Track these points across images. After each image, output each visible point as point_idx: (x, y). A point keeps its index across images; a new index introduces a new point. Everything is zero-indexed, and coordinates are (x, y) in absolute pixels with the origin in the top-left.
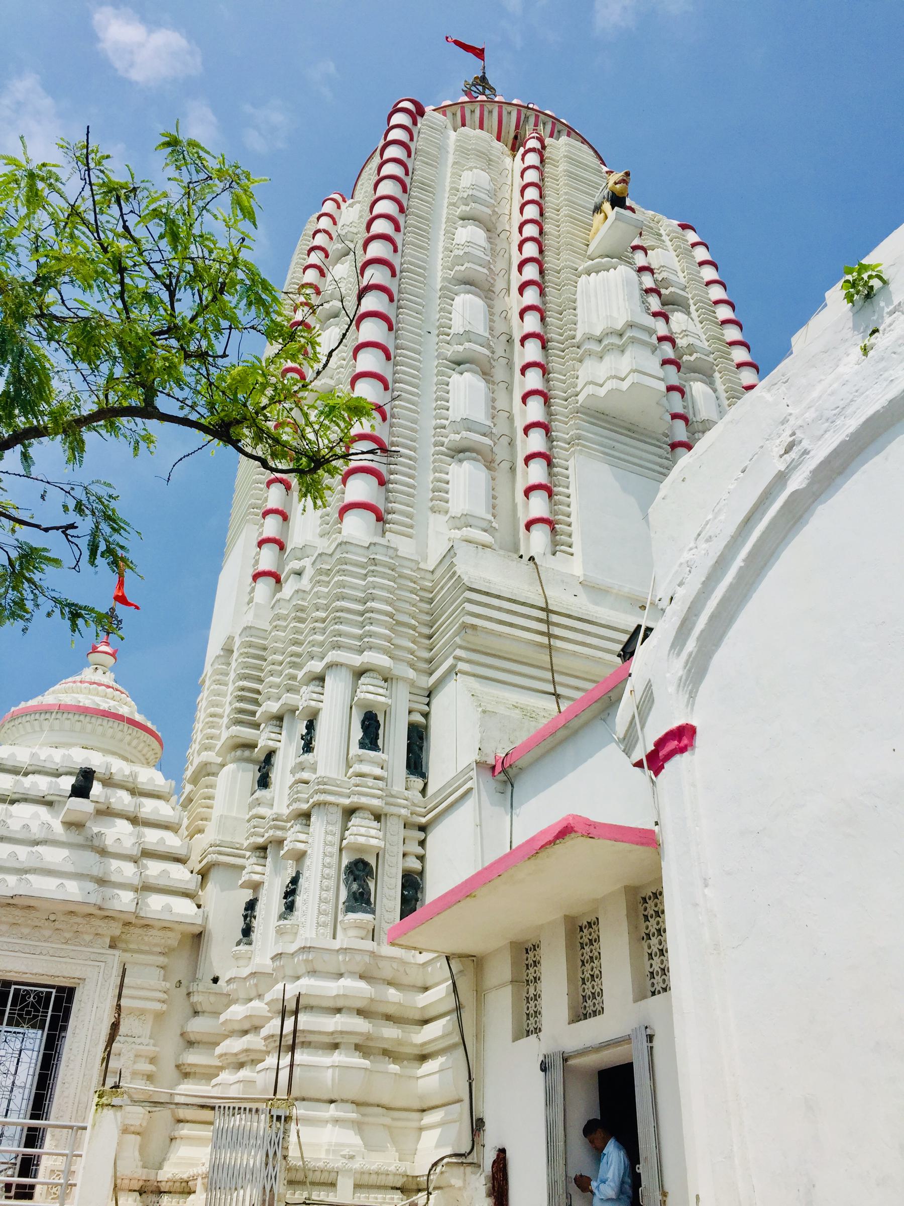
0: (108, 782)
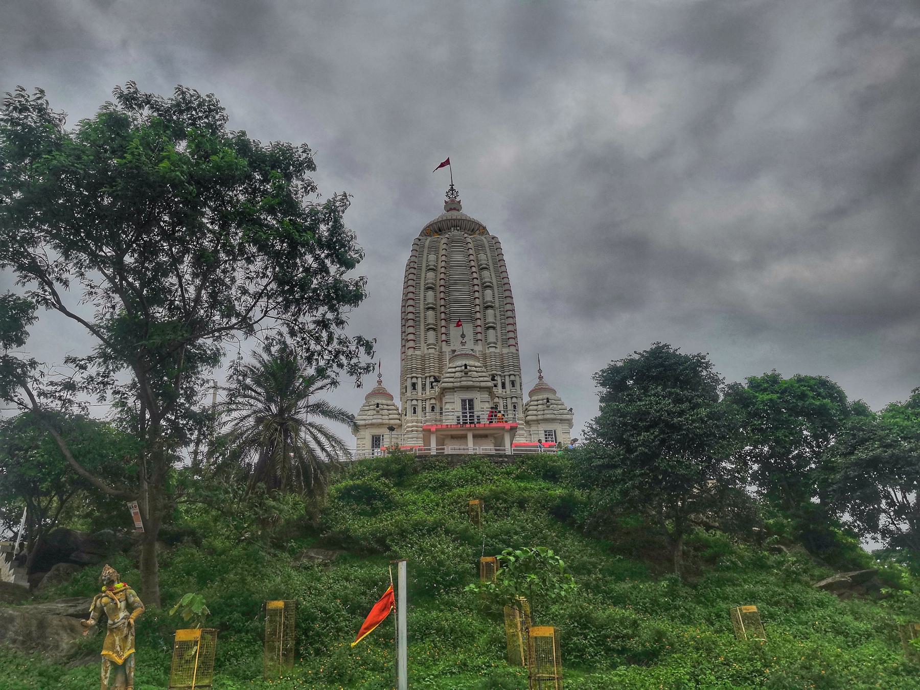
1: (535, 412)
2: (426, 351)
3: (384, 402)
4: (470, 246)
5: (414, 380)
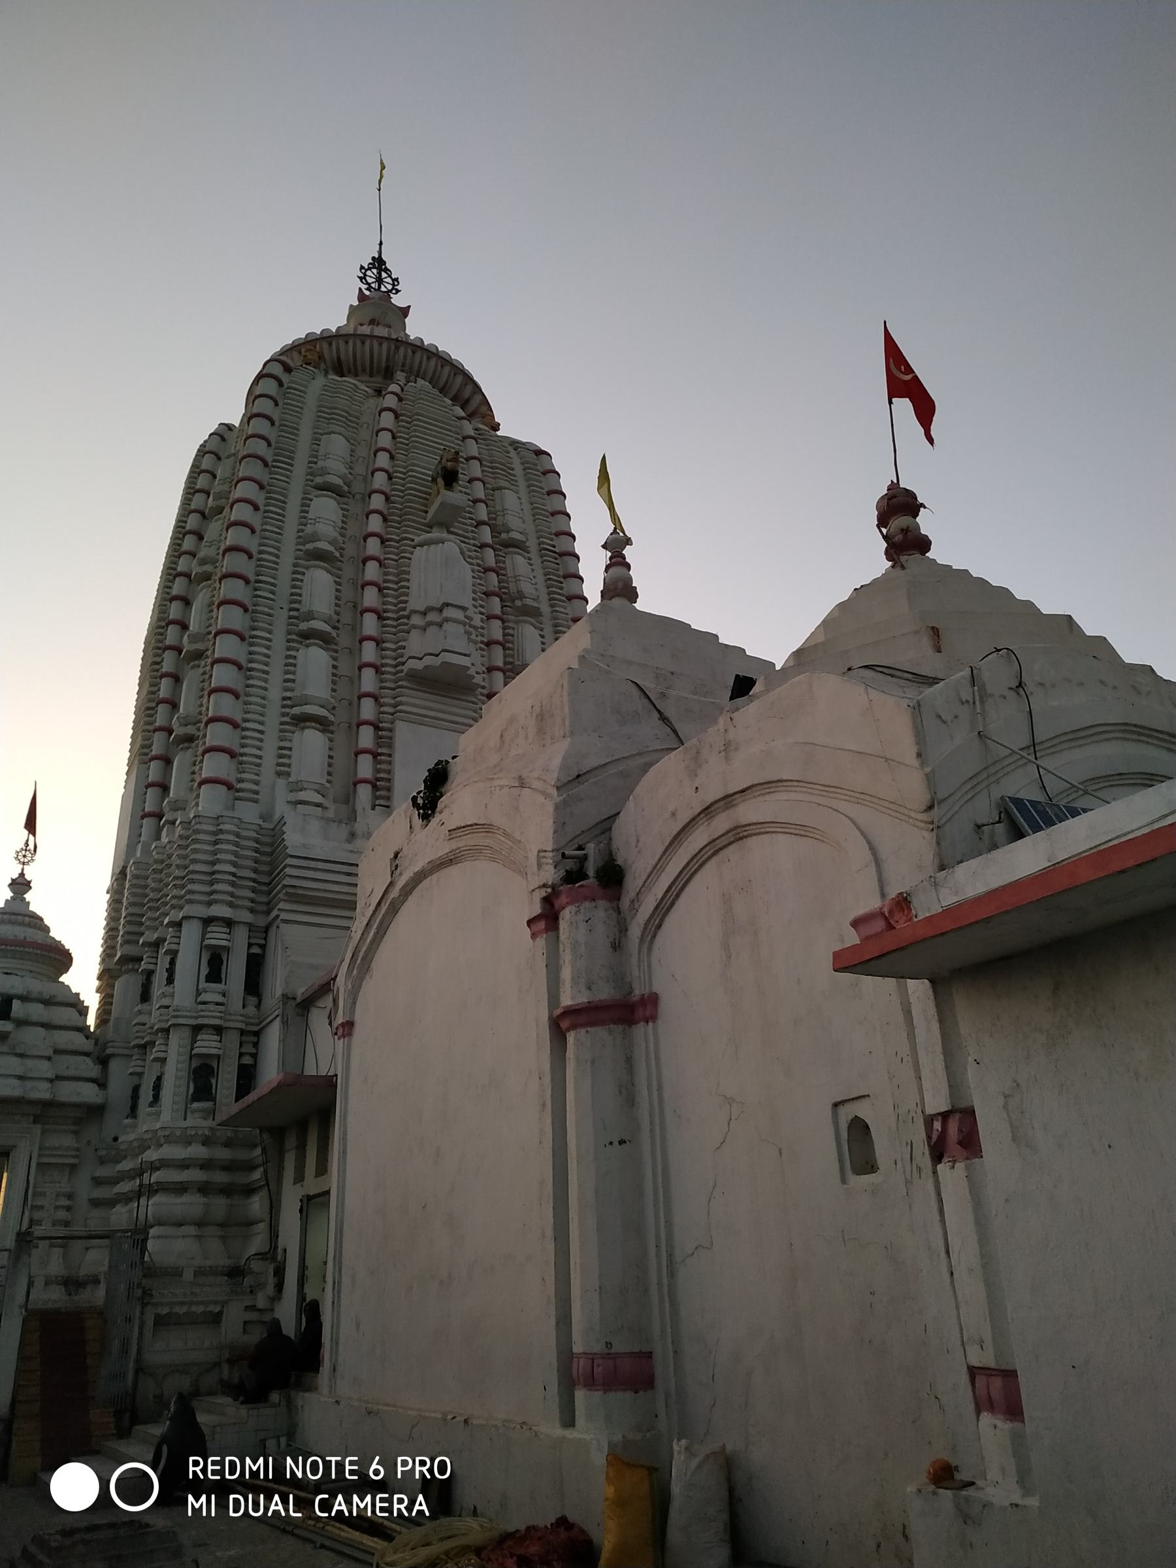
0: (24, 999)
5: (218, 936)
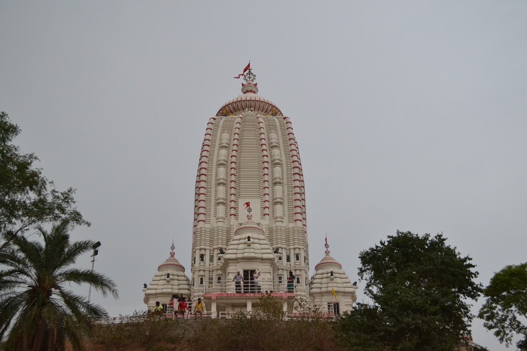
1: (319, 285)
2: (215, 225)
3: (175, 273)
4: (261, 125)
5: (203, 252)
